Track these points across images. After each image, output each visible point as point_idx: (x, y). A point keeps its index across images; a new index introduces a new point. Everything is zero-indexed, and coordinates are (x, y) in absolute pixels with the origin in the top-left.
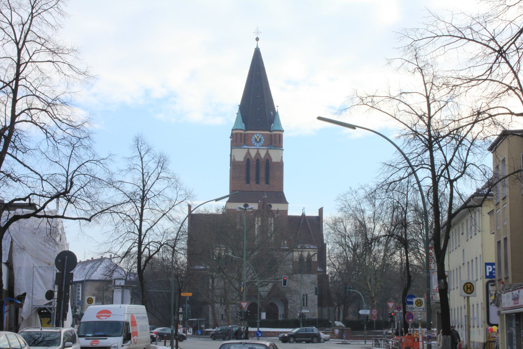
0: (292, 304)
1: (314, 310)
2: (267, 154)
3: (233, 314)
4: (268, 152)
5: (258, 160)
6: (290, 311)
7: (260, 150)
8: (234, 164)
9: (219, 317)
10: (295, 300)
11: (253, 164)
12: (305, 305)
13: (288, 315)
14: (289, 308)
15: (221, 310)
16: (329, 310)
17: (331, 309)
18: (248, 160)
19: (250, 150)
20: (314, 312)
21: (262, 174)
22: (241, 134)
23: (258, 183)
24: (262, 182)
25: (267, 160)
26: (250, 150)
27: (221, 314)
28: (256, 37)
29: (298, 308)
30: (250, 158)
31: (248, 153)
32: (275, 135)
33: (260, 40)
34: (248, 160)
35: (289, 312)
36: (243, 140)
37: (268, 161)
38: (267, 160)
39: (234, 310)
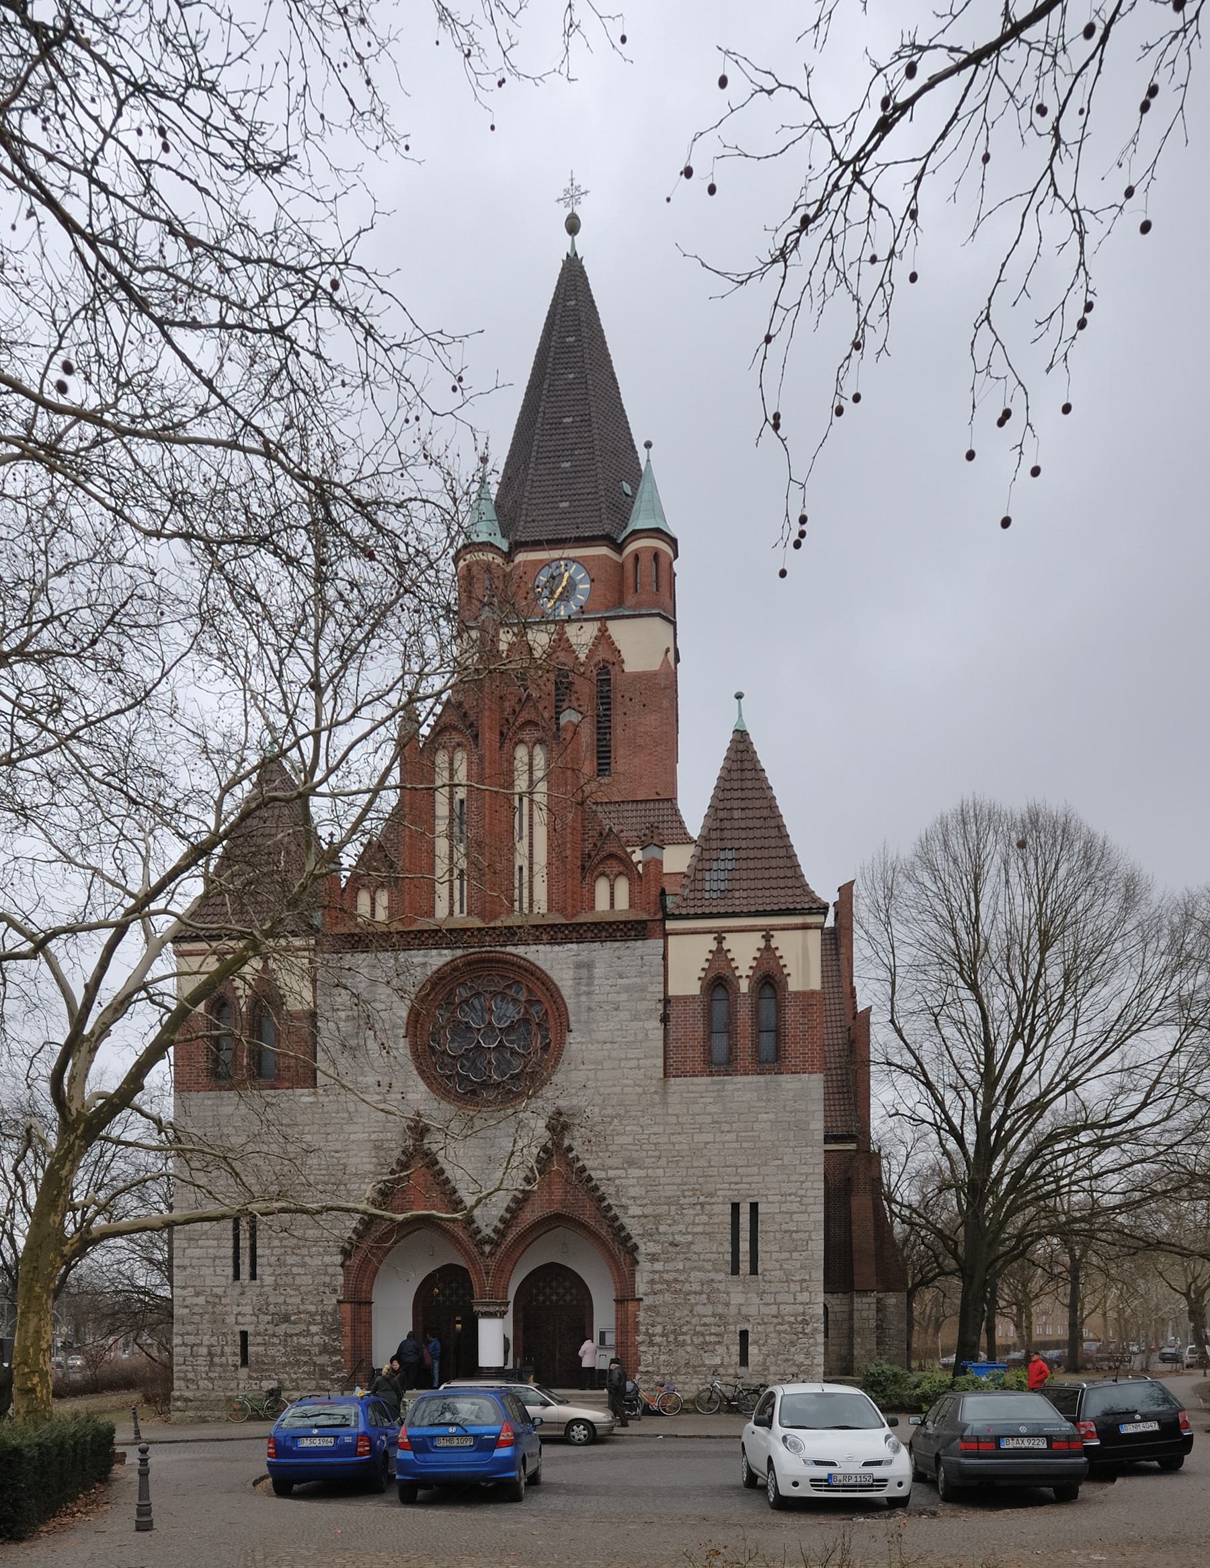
0: (658, 1266)
1: (804, 1297)
2: (603, 637)
3: (308, 1333)
4: (606, 630)
6: (649, 1308)
9: (227, 1349)
10: (678, 1238)
12: (745, 1266)
13: (637, 1331)
14: (641, 1288)
15: (236, 1310)
16: (881, 1307)
17: (892, 1300)
20: (800, 1308)
22: (488, 568)
27: (238, 1329)
29: (696, 1287)
35: (642, 1317)
39: (312, 1308)
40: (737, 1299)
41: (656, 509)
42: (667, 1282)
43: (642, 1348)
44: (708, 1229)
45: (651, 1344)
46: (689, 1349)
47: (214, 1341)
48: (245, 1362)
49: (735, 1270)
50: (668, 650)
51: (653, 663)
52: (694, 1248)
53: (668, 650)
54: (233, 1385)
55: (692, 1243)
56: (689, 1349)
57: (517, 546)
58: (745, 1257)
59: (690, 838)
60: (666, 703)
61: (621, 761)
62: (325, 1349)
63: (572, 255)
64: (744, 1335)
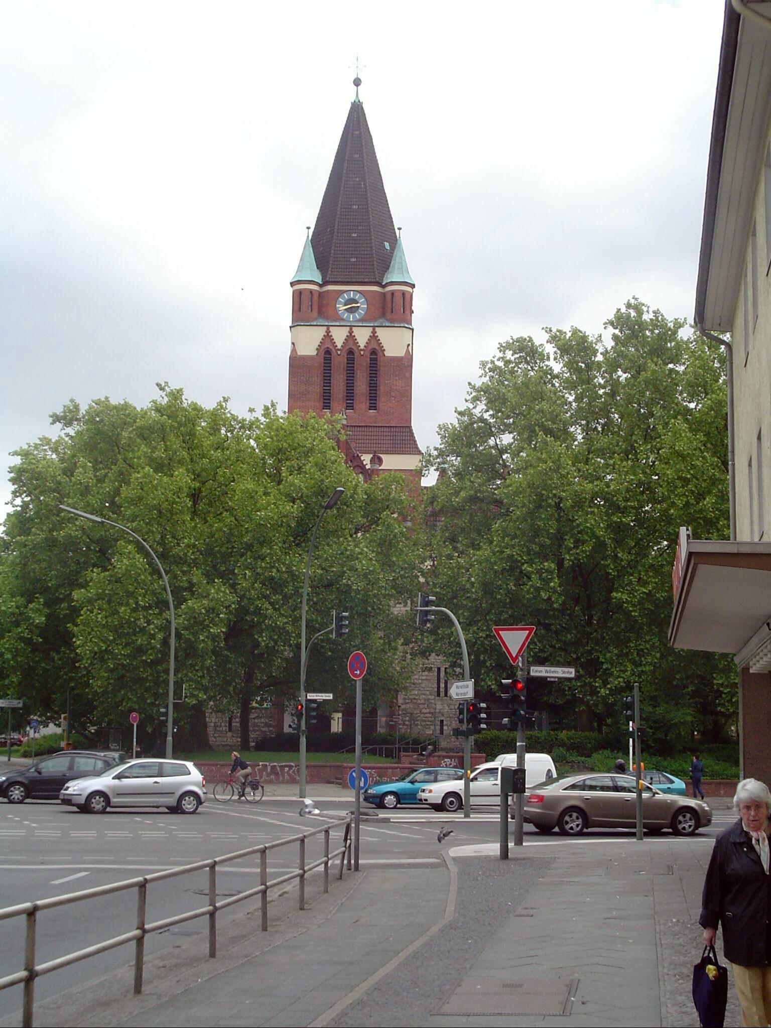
2: (374, 337)
5: (351, 352)
6: (403, 710)
7: (354, 329)
8: (297, 364)
9: (223, 724)
11: (339, 361)
12: (442, 694)
18: (328, 352)
19: (331, 328)
21: (361, 385)
22: (311, 291)
23: (350, 407)
24: (362, 403)
25: (374, 352)
26: (331, 328)
28: (355, 77)
29: (422, 701)
30: (331, 347)
31: (328, 336)
32: (393, 293)
33: (362, 84)
34: (326, 351)
36: (315, 307)
37: (376, 354)
38: (374, 352)
40: (439, 707)
41: (404, 269)
42: (411, 699)
43: (401, 726)
44: (428, 678)
45: (404, 724)
46: (419, 727)
47: (217, 720)
48: (230, 730)
49: (439, 695)
50: (409, 345)
51: (401, 353)
52: (422, 685)
53: (409, 345)
54: (225, 739)
55: (421, 683)
56: (419, 727)
57: (325, 283)
58: (442, 690)
59: (420, 451)
60: (407, 375)
61: (382, 403)
62: (266, 725)
63: (357, 101)
64: (442, 721)
